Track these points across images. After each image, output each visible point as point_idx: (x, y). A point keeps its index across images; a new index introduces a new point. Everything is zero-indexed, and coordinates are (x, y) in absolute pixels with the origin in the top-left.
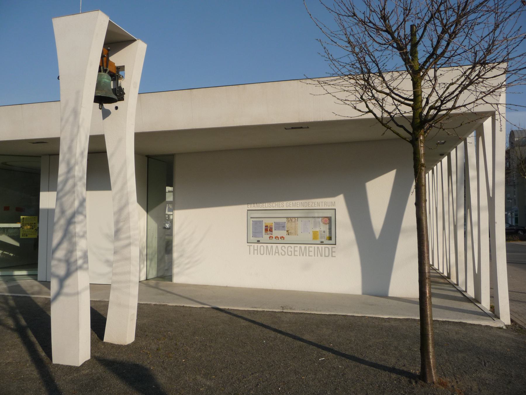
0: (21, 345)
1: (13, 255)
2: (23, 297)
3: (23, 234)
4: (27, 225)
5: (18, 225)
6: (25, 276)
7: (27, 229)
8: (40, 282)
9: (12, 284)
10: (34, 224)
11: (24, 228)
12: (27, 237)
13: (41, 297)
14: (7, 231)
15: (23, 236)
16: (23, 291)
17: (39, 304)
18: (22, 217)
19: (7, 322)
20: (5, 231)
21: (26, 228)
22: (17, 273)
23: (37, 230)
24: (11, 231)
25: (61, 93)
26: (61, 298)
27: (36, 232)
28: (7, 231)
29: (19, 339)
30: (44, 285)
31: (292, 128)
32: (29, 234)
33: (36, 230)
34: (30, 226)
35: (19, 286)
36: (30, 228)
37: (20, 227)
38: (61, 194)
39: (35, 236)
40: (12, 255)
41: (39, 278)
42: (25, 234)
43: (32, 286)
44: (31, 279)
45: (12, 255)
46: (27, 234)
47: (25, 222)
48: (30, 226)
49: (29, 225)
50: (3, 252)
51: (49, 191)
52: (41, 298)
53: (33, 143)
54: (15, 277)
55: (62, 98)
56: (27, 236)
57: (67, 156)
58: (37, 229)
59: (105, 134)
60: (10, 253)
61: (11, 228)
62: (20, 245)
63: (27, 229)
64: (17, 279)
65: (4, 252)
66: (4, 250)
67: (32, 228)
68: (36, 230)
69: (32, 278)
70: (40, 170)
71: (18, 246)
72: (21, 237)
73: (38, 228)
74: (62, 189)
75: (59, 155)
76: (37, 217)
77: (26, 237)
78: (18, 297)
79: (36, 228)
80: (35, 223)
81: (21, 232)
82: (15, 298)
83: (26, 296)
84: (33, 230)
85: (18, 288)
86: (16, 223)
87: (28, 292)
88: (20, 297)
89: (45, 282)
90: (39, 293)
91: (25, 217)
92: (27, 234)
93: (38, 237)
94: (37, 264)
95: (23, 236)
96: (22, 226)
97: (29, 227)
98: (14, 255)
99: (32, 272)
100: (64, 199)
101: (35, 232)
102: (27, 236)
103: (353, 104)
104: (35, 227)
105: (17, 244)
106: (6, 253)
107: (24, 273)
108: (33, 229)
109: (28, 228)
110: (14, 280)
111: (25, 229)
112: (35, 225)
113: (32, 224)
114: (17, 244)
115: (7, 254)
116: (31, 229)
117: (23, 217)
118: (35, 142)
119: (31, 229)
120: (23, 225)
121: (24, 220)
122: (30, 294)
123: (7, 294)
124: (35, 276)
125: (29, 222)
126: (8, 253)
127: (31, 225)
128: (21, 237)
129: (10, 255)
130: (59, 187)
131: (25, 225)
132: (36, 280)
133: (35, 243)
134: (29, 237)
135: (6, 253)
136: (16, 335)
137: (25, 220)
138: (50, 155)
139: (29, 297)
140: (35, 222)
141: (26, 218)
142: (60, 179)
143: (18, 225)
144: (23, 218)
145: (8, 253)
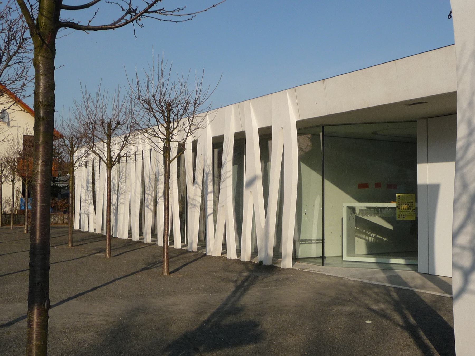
0: (415, 348)
1: (387, 240)
2: (405, 289)
3: (400, 215)
4: (403, 205)
5: (394, 205)
6: (403, 266)
7: (404, 209)
8: (420, 273)
9: (390, 274)
10: (411, 204)
11: (400, 208)
12: (405, 219)
13: (426, 292)
14: (381, 211)
15: (399, 217)
16: (405, 284)
17: (425, 300)
18: (397, 195)
19: (394, 318)
20: (379, 212)
21: (402, 208)
22: (393, 261)
23: (416, 210)
24: (385, 211)
25: (456, 34)
26: (466, 297)
27: (414, 213)
28: (381, 211)
29: (411, 340)
30: (425, 277)
31: (414, 104)
32: (406, 215)
33: (414, 211)
34: (407, 206)
35: (398, 276)
36: (407, 208)
37: (396, 207)
38: (461, 163)
39: (414, 219)
40: (385, 239)
41: (420, 269)
42: (402, 215)
43: (413, 278)
44: (410, 269)
45: (385, 239)
46: (404, 215)
47: (401, 201)
48: (407, 206)
49: (406, 205)
50: (376, 235)
51: (427, 163)
52: (427, 293)
53: (409, 105)
54: (392, 266)
55: (458, 40)
56: (404, 217)
57: (468, 114)
58: (415, 210)
59: (457, 92)
60: (383, 237)
61: (387, 207)
62: (393, 228)
63: (404, 209)
64: (394, 268)
65: (377, 236)
66: (377, 234)
67: (409, 208)
68: (414, 211)
69: (409, 267)
70: (416, 138)
71: (391, 230)
72: (398, 219)
73: (417, 208)
74: (462, 157)
75: (456, 114)
76: (414, 195)
77: (402, 219)
78: (399, 289)
79: (414, 208)
80: (412, 203)
81: (397, 213)
82: (398, 290)
83: (409, 290)
84: (410, 211)
85: (395, 279)
86: (390, 202)
87: (412, 284)
88: (402, 289)
89: (427, 275)
90: (423, 287)
91: (401, 194)
92: (404, 215)
93: (417, 218)
94: (417, 251)
95: (399, 217)
96: (398, 206)
97: (406, 207)
98: (388, 240)
99: (410, 262)
100: (466, 170)
101: (413, 213)
102: (404, 217)
103: (126, 122)
104: (412, 207)
105: (390, 227)
106: (379, 237)
107: (402, 261)
108: (410, 209)
109: (405, 208)
110: (391, 269)
111: (402, 209)
112: (413, 205)
113: (409, 204)
114: (390, 227)
115: (380, 238)
116: (408, 209)
117: (399, 194)
118: (411, 104)
119: (408, 209)
120: (399, 205)
121: (400, 198)
122: (412, 288)
123: (387, 285)
124: (415, 267)
125: (406, 201)
126: (381, 238)
127: (408, 205)
128: (398, 219)
129: (384, 240)
130: (459, 155)
131: (402, 205)
132: (417, 271)
133: (414, 225)
134: (406, 218)
135: (379, 237)
136: (406, 334)
137: (401, 198)
138: (427, 118)
139: (413, 291)
140: (412, 201)
141: (402, 196)
142: (459, 144)
143: (394, 205)
144: (399, 196)
145: (381, 238)
